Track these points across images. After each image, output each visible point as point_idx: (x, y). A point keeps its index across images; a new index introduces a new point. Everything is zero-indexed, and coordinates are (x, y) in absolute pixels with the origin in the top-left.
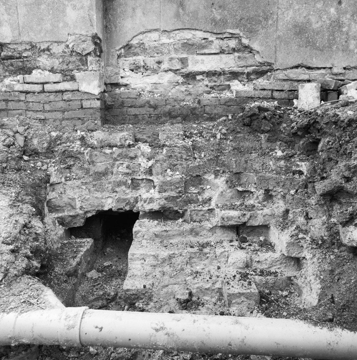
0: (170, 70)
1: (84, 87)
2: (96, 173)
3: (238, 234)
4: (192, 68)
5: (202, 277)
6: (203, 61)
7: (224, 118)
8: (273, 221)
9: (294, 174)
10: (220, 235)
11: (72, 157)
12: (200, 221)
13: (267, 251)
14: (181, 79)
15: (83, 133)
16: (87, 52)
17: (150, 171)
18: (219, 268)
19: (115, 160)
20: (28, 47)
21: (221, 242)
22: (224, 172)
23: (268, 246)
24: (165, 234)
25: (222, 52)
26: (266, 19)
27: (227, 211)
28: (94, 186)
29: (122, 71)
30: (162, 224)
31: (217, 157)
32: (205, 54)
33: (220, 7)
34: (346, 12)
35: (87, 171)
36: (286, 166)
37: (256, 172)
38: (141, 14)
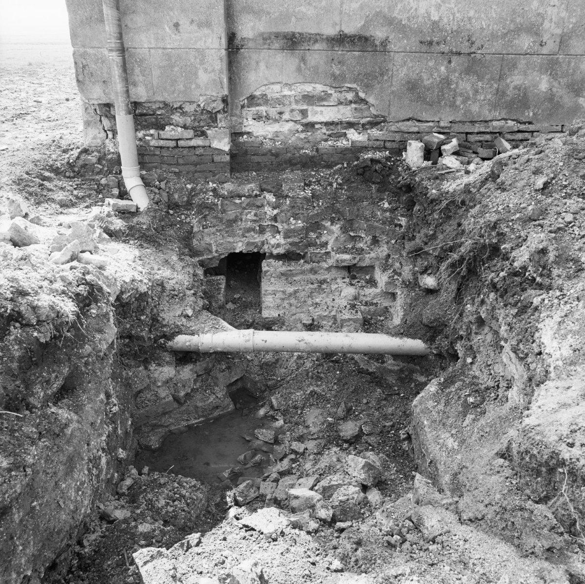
0: (292, 120)
1: (215, 144)
2: (228, 221)
3: (349, 272)
4: (311, 118)
5: (321, 307)
6: (322, 112)
7: (340, 166)
8: (378, 262)
9: (396, 226)
10: (334, 273)
11: (207, 207)
12: (318, 262)
13: (371, 287)
14: (300, 128)
15: (215, 185)
16: (216, 110)
17: (275, 218)
18: (334, 300)
19: (244, 209)
20: (161, 106)
21: (336, 279)
22: (339, 219)
23: (372, 283)
24: (289, 273)
25: (340, 103)
26: (382, 75)
27: (341, 255)
28: (227, 232)
29: (245, 120)
30: (286, 264)
31: (333, 204)
32: (324, 106)
33: (339, 62)
34: (455, 71)
35: (221, 220)
36: (391, 217)
37: (367, 220)
38: (265, 67)
